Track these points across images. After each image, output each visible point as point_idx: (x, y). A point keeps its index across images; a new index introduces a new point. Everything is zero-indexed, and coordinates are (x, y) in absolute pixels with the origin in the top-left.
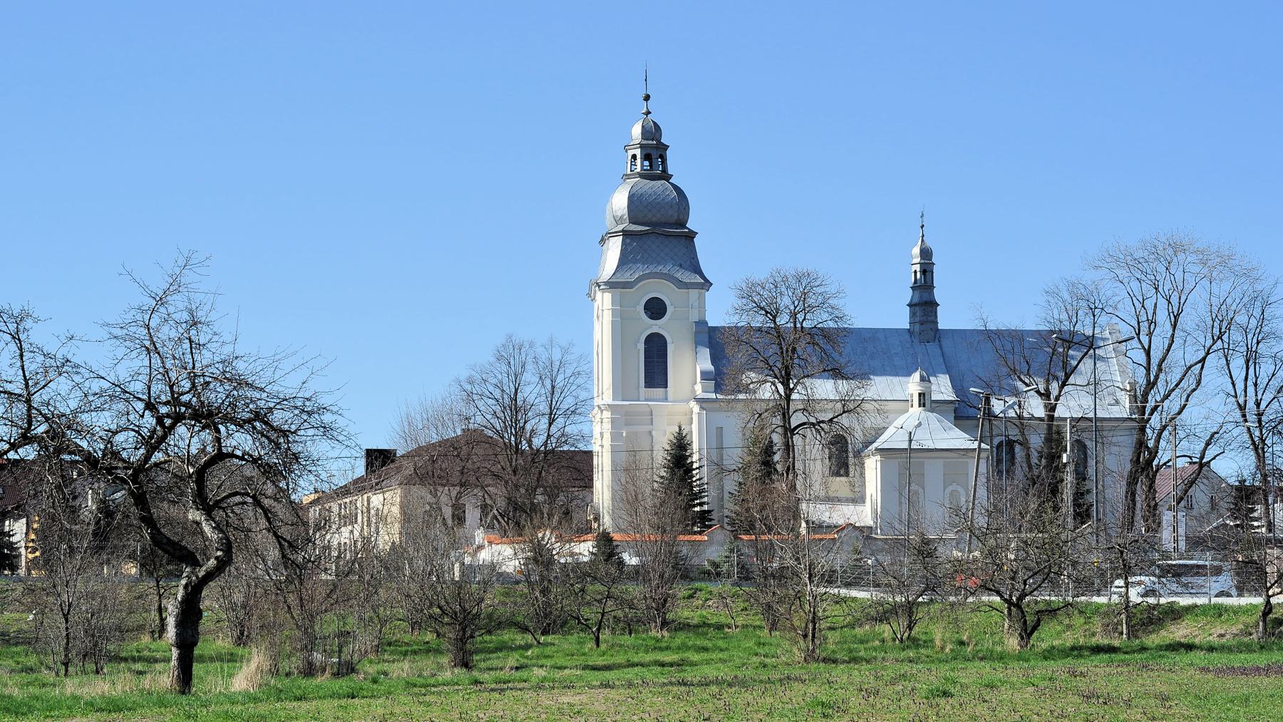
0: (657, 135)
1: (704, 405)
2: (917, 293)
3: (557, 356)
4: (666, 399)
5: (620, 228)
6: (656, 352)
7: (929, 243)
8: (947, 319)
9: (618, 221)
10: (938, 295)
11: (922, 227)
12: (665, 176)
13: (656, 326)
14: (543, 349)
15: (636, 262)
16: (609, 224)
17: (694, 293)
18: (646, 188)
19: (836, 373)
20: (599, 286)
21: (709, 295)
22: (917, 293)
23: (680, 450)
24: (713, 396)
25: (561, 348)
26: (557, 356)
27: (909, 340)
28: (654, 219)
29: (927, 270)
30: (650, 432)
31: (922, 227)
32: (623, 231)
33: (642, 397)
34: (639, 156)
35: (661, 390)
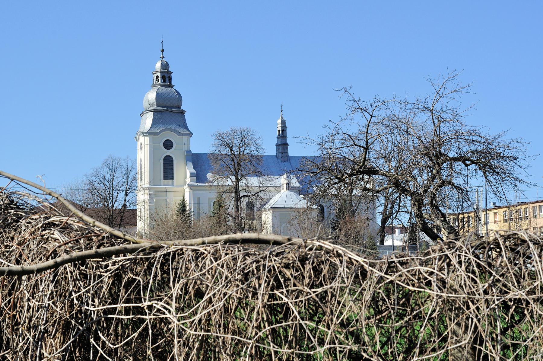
0: (168, 67)
1: (192, 188)
2: (280, 140)
3: (130, 165)
4: (173, 185)
5: (152, 108)
6: (168, 163)
7: (284, 118)
8: (292, 152)
9: (151, 105)
10: (289, 141)
11: (282, 111)
12: (171, 86)
13: (169, 153)
14: (124, 161)
15: (159, 124)
16: (146, 106)
17: (185, 138)
18: (164, 91)
19: (259, 174)
20: (143, 134)
21: (192, 139)
22: (280, 140)
23: (183, 206)
24: (196, 184)
25: (132, 161)
26: (130, 165)
27: (277, 160)
28: (167, 105)
29: (284, 130)
30: (166, 200)
31: (282, 111)
32: (154, 110)
33: (162, 184)
34: (160, 77)
35: (171, 181)
